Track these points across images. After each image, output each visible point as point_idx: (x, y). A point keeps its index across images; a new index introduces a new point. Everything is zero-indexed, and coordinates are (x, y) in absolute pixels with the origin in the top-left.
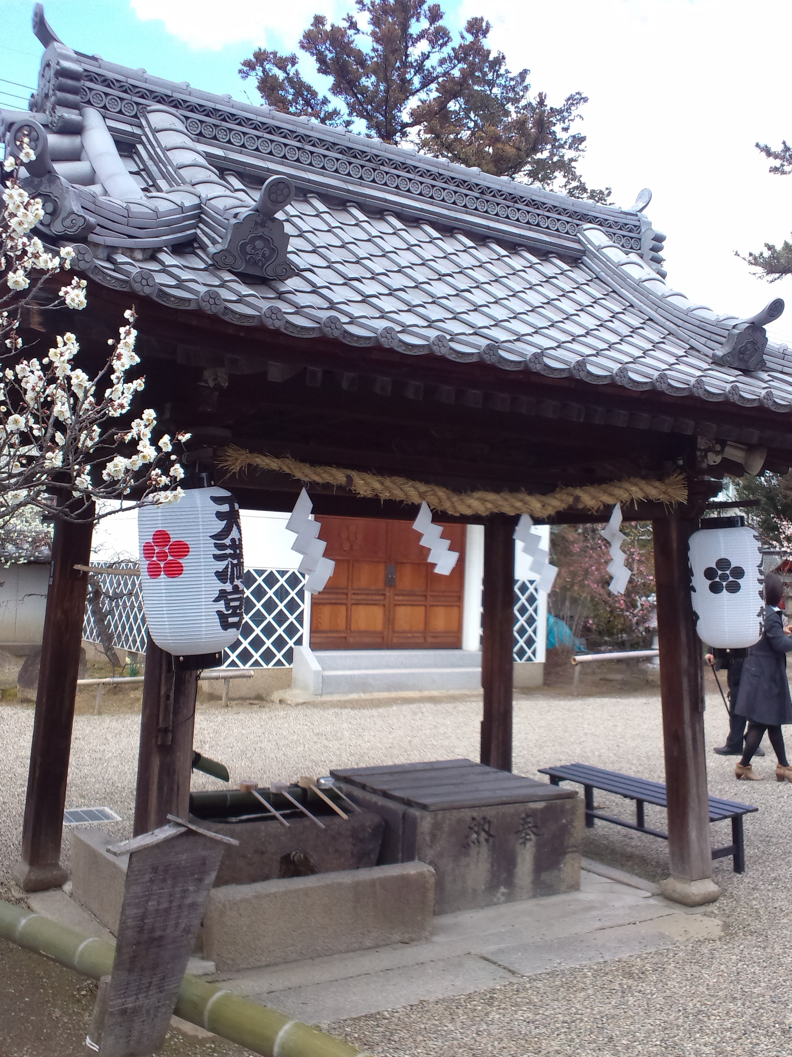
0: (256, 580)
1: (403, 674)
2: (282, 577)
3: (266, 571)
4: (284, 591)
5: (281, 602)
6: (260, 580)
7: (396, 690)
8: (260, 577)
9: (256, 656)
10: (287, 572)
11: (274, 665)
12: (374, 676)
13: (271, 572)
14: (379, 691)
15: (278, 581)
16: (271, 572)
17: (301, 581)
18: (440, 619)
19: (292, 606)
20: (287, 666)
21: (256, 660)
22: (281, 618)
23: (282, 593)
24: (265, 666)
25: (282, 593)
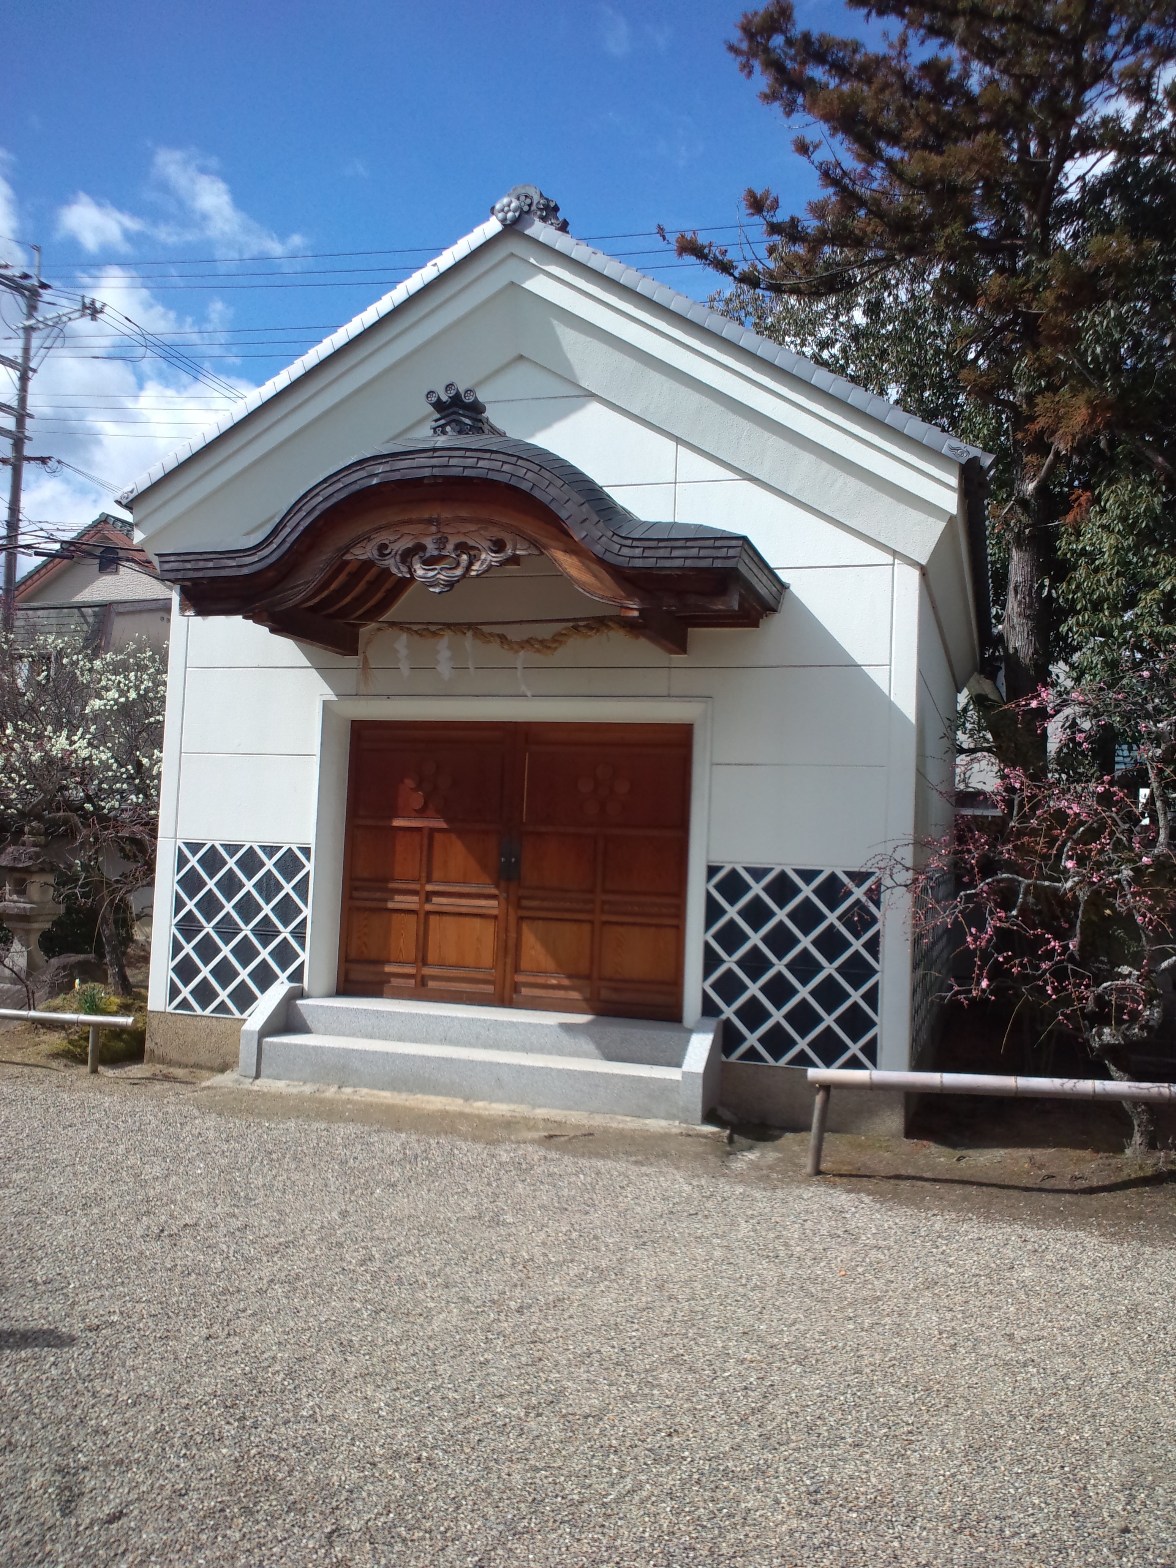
0: (225, 863)
1: (427, 1059)
2: (270, 858)
3: (820, 872)
4: (272, 882)
5: (267, 903)
6: (231, 863)
7: (410, 1091)
8: (231, 857)
9: (223, 995)
10: (818, 873)
11: (791, 1062)
12: (363, 1055)
13: (213, 846)
14: (373, 1086)
15: (263, 864)
16: (213, 846)
17: (304, 866)
18: (632, 954)
19: (287, 911)
20: (237, 1014)
21: (223, 1002)
22: (266, 932)
23: (268, 887)
24: (199, 1011)
25: (268, 887)
